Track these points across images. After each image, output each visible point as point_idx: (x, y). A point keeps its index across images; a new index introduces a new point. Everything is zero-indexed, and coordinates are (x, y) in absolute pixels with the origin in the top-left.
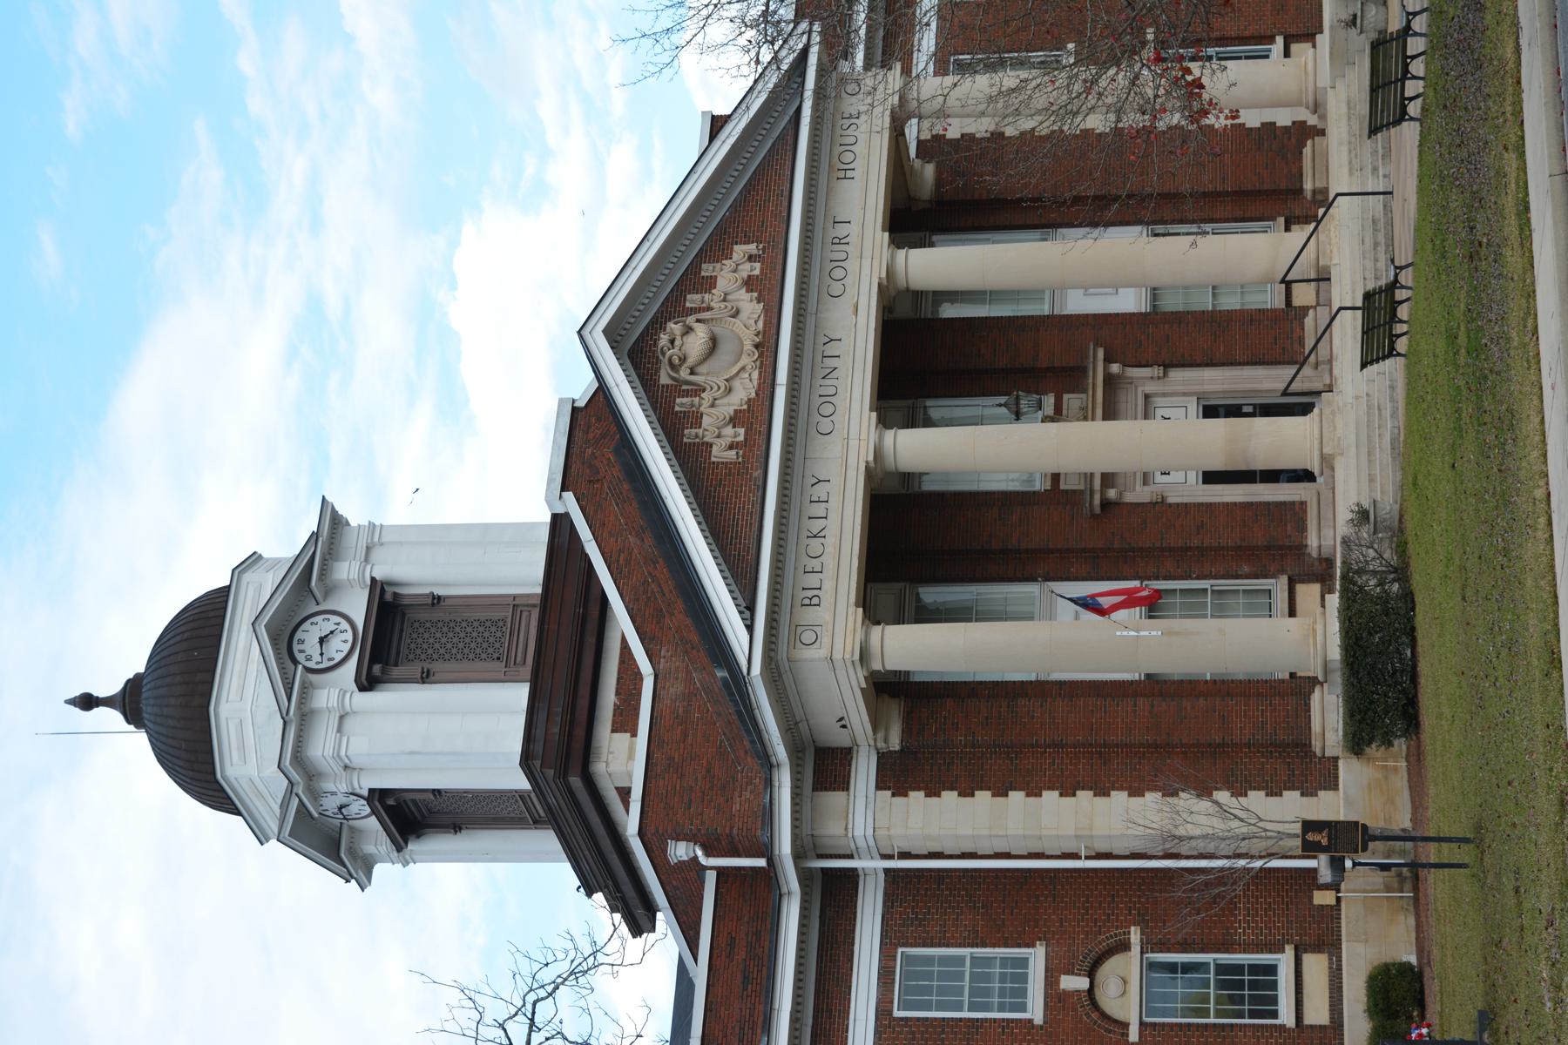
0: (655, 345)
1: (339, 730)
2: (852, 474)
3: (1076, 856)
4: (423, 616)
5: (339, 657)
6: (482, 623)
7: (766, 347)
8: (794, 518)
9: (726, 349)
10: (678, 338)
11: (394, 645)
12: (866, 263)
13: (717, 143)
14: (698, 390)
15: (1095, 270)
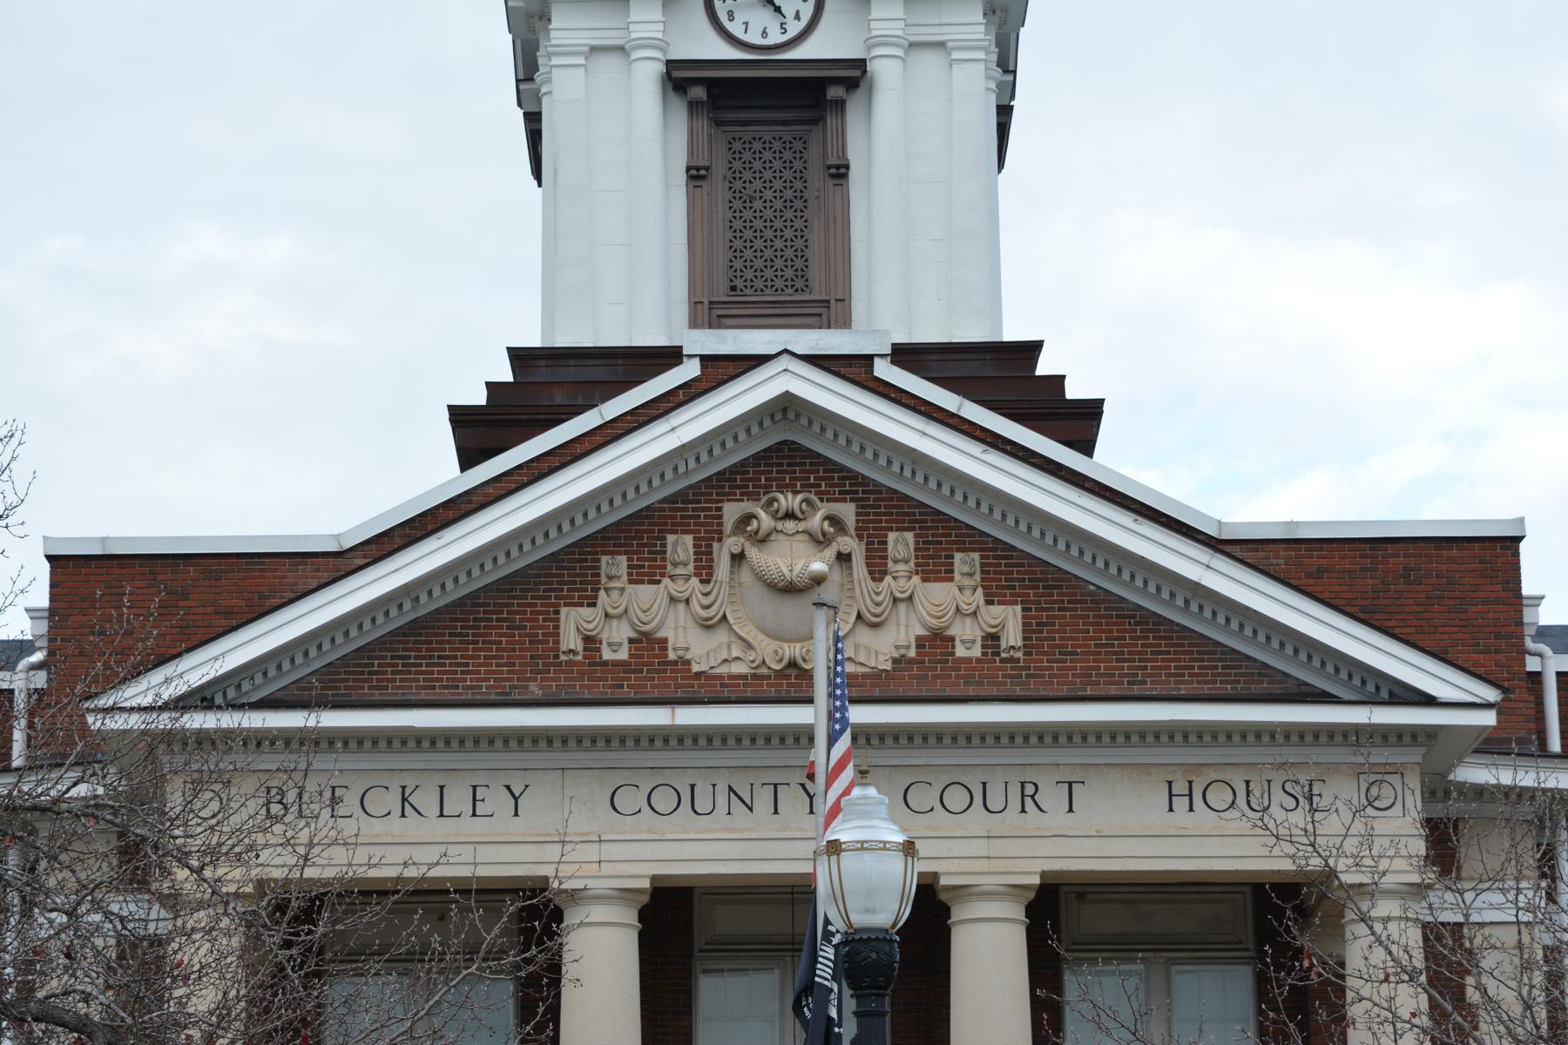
1: (595, 49)
2: (530, 853)
4: (813, 155)
5: (735, 28)
8: (366, 761)
9: (789, 612)
10: (801, 526)
12: (979, 848)
13: (1202, 554)
14: (705, 571)
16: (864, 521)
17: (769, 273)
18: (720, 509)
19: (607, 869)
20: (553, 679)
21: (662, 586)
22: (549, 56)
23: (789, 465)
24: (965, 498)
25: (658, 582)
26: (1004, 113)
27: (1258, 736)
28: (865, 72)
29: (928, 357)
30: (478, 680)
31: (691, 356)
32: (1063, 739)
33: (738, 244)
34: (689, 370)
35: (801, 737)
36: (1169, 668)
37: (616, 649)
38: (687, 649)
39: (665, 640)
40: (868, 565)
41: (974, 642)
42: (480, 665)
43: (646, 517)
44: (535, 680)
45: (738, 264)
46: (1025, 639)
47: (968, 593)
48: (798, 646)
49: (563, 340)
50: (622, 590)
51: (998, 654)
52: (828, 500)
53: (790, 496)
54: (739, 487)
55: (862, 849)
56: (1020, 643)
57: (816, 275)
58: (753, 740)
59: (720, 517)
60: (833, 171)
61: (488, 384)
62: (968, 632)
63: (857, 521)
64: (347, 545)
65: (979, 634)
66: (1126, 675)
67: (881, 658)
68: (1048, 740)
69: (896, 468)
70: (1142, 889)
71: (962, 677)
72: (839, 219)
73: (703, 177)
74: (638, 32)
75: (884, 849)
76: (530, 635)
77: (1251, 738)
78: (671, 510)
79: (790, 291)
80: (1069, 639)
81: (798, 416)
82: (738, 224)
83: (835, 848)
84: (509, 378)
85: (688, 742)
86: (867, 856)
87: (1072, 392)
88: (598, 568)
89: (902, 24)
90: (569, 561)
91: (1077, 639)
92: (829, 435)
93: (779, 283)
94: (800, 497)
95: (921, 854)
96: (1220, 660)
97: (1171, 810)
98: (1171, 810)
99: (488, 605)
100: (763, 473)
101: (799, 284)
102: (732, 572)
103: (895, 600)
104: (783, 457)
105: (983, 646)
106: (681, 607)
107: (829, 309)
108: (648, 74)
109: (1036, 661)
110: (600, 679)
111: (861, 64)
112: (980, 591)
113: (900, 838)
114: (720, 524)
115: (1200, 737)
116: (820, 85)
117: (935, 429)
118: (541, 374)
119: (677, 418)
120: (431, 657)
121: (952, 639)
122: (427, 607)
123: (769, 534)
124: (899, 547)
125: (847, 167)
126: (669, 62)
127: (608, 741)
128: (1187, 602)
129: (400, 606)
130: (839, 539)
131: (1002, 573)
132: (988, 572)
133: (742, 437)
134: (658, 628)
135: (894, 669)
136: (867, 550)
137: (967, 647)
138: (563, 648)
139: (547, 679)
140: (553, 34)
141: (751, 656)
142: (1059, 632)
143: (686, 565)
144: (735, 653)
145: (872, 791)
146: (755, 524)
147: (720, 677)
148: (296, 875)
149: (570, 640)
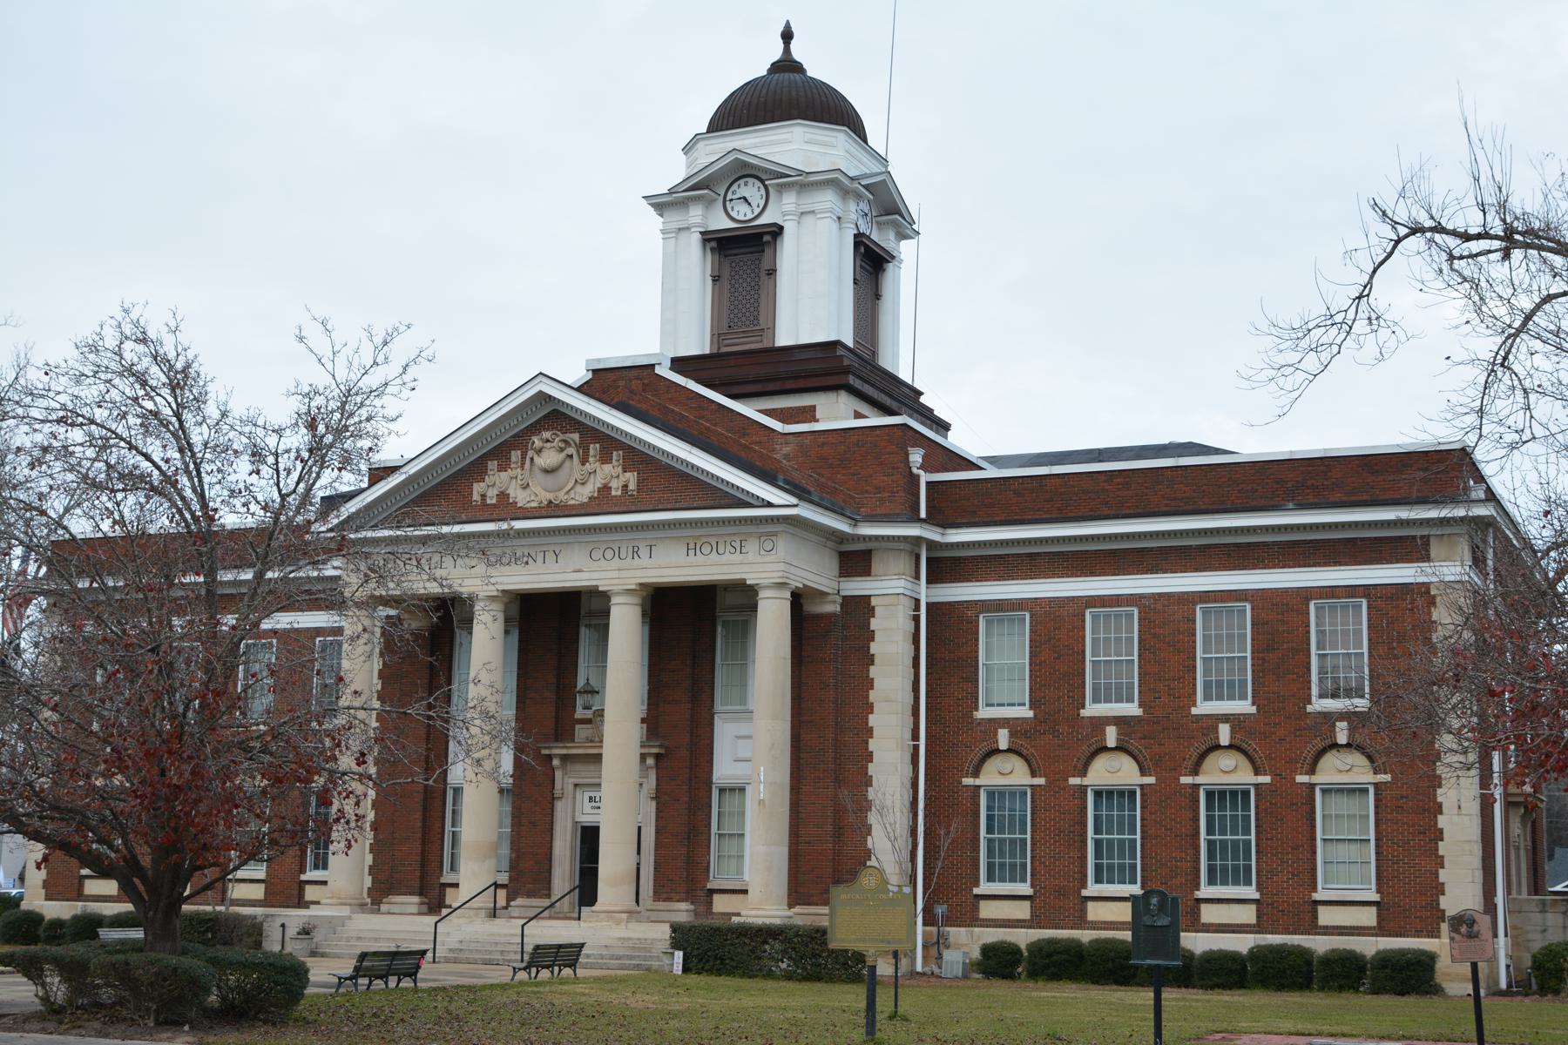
3: (916, 748)
5: (734, 214)
7: (553, 509)
12: (615, 574)
15: (751, 746)
108: (696, 238)
116: (761, 235)
122: (678, 466)
149: (476, 497)
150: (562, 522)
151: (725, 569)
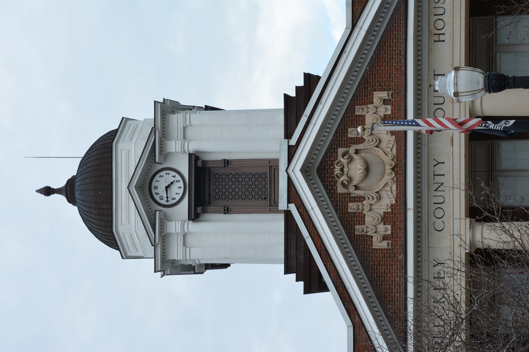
0: (333, 173)
1: (184, 245)
4: (221, 171)
5: (178, 197)
6: (254, 175)
7: (399, 168)
9: (375, 170)
10: (346, 166)
11: (207, 189)
13: (357, 30)
14: (361, 199)
16: (344, 145)
17: (260, 186)
18: (340, 194)
19: (463, 233)
20: (397, 251)
21: (366, 213)
22: (186, 260)
23: (325, 171)
24: (337, 110)
25: (364, 215)
26: (207, 108)
27: (419, 11)
28: (193, 154)
29: (289, 132)
30: (395, 77)
31: (288, 207)
32: (419, 170)
33: (250, 197)
34: (293, 208)
35: (418, 135)
36: (395, 42)
37: (387, 229)
38: (387, 205)
39: (384, 212)
40: (359, 144)
41: (386, 108)
42: (392, 276)
43: (342, 219)
44: (397, 257)
45: (257, 197)
46: (385, 91)
47: (369, 110)
48: (386, 167)
49: (282, 256)
50: (367, 227)
51: (390, 100)
52: (337, 157)
53: (335, 170)
54: (332, 187)
55: (457, 84)
56: (387, 92)
57: (261, 171)
58: (419, 183)
59: (342, 194)
60: (226, 165)
61: (296, 281)
62: (382, 110)
63: (344, 147)
64: (351, 324)
65: (383, 106)
66: (398, 56)
67: (391, 139)
68: (420, 82)
69: (326, 134)
70: (471, 54)
71: (398, 112)
72: (242, 163)
73: (228, 208)
74: (179, 230)
75: (457, 77)
76: (382, 259)
77: (420, 14)
78: (340, 210)
79: (266, 179)
80: (385, 75)
81: (308, 167)
82: (243, 197)
83: (456, 94)
84: (295, 274)
85: (419, 175)
86: (459, 83)
87: (301, 84)
88: (359, 235)
89: (177, 141)
90: (357, 245)
91: (385, 73)
92: (315, 156)
93: (263, 183)
94: (336, 166)
95: (459, 65)
96: (393, 25)
97: (444, 41)
98: (444, 41)
99: (372, 273)
100: (327, 179)
101: (264, 176)
102: (361, 190)
103: (371, 134)
104: (322, 172)
105: (387, 105)
106: (373, 207)
107: (272, 166)
108: (193, 227)
109: (393, 87)
110: (397, 235)
111: (190, 155)
112: (368, 106)
113: (453, 72)
114: (345, 194)
115: (419, 31)
116: (197, 169)
117: (313, 121)
118: (293, 263)
119: (308, 207)
120: (389, 292)
121: (385, 115)
122: (372, 293)
123: (348, 177)
124: (353, 133)
125: (225, 160)
126: (189, 219)
127: (419, 232)
128: (373, 36)
129: (372, 302)
130: (350, 153)
131: (362, 98)
132: (362, 103)
133: (315, 186)
134: (380, 215)
135: (395, 135)
136: (354, 144)
137: (388, 110)
138: (387, 247)
139: (397, 253)
140: (179, 259)
141: (390, 183)
142: (383, 79)
143: (359, 205)
144: (389, 189)
145: (437, 83)
146: (345, 181)
147: (397, 194)
148: (464, 274)
149: (384, 245)
150: (411, 163)
151: (457, 21)
